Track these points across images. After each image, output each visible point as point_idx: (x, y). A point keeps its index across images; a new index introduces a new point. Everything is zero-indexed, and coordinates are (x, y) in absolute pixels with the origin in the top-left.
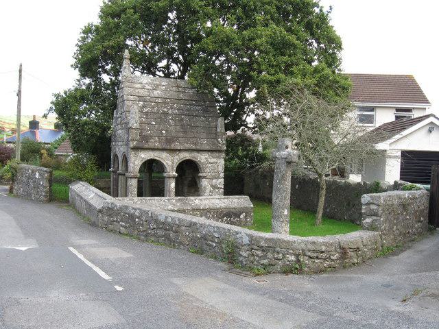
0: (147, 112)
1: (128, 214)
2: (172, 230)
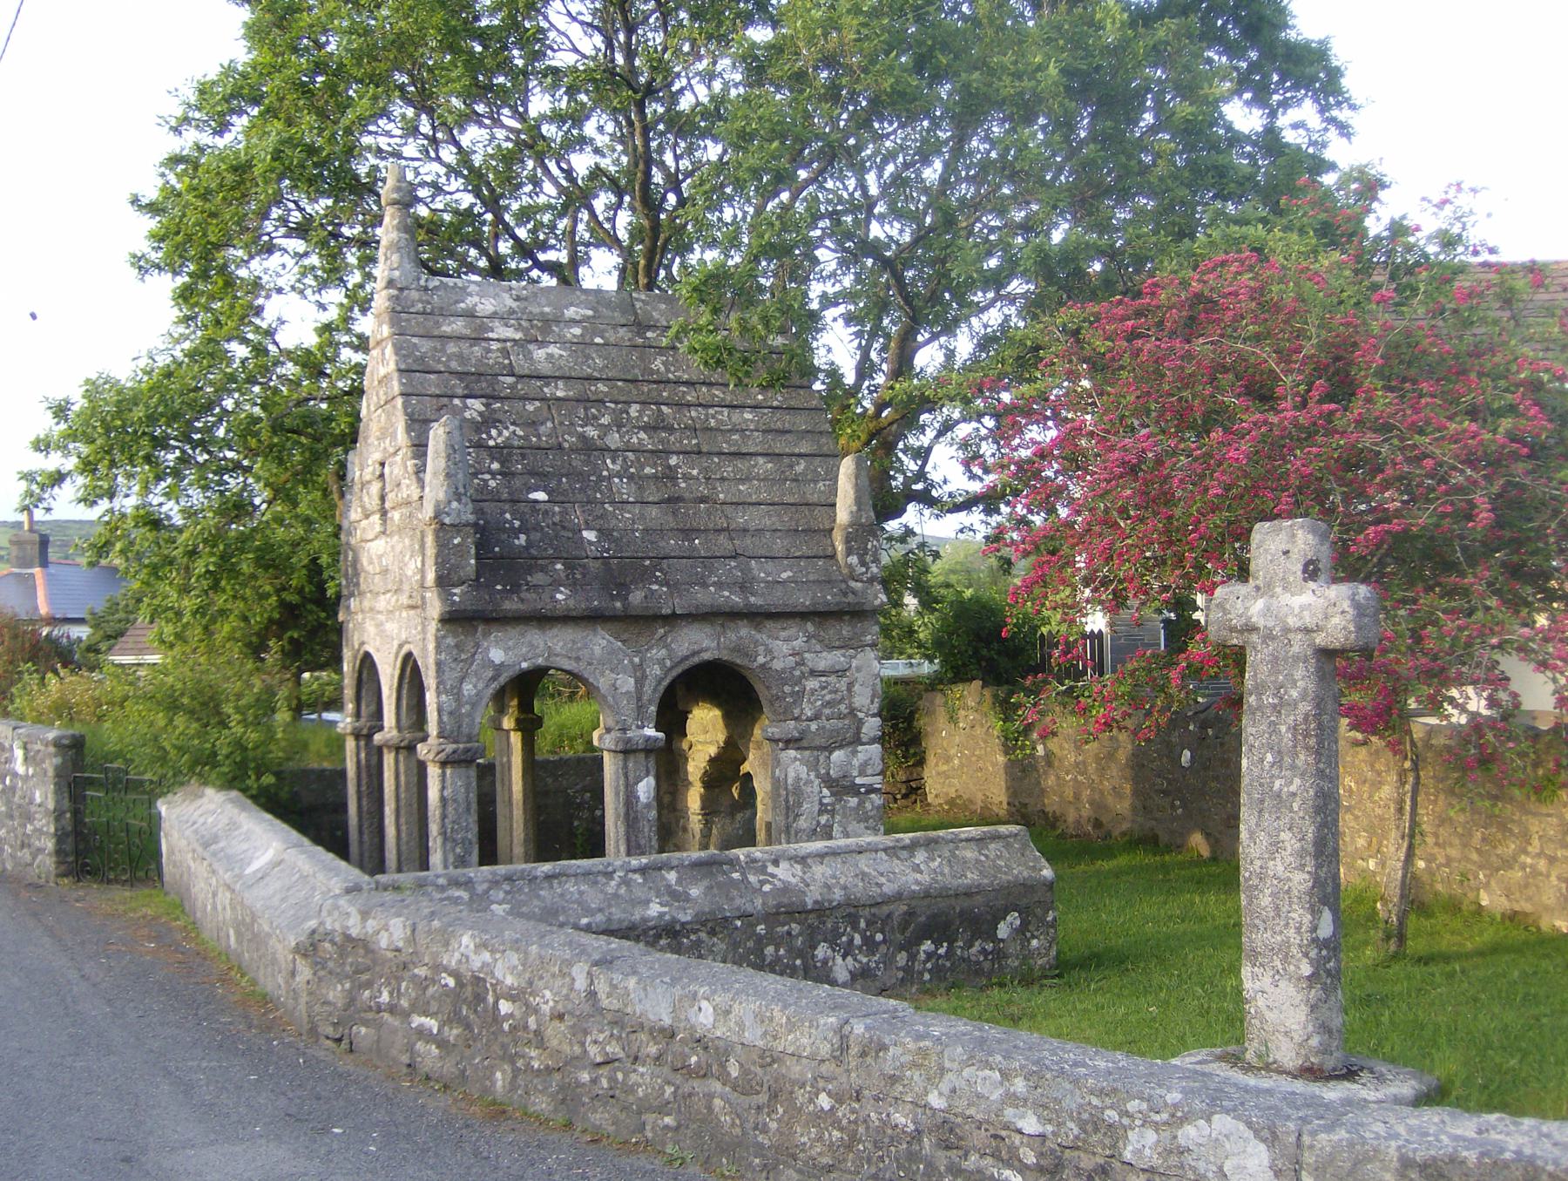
0: (507, 446)
1: (456, 974)
2: (724, 1077)
